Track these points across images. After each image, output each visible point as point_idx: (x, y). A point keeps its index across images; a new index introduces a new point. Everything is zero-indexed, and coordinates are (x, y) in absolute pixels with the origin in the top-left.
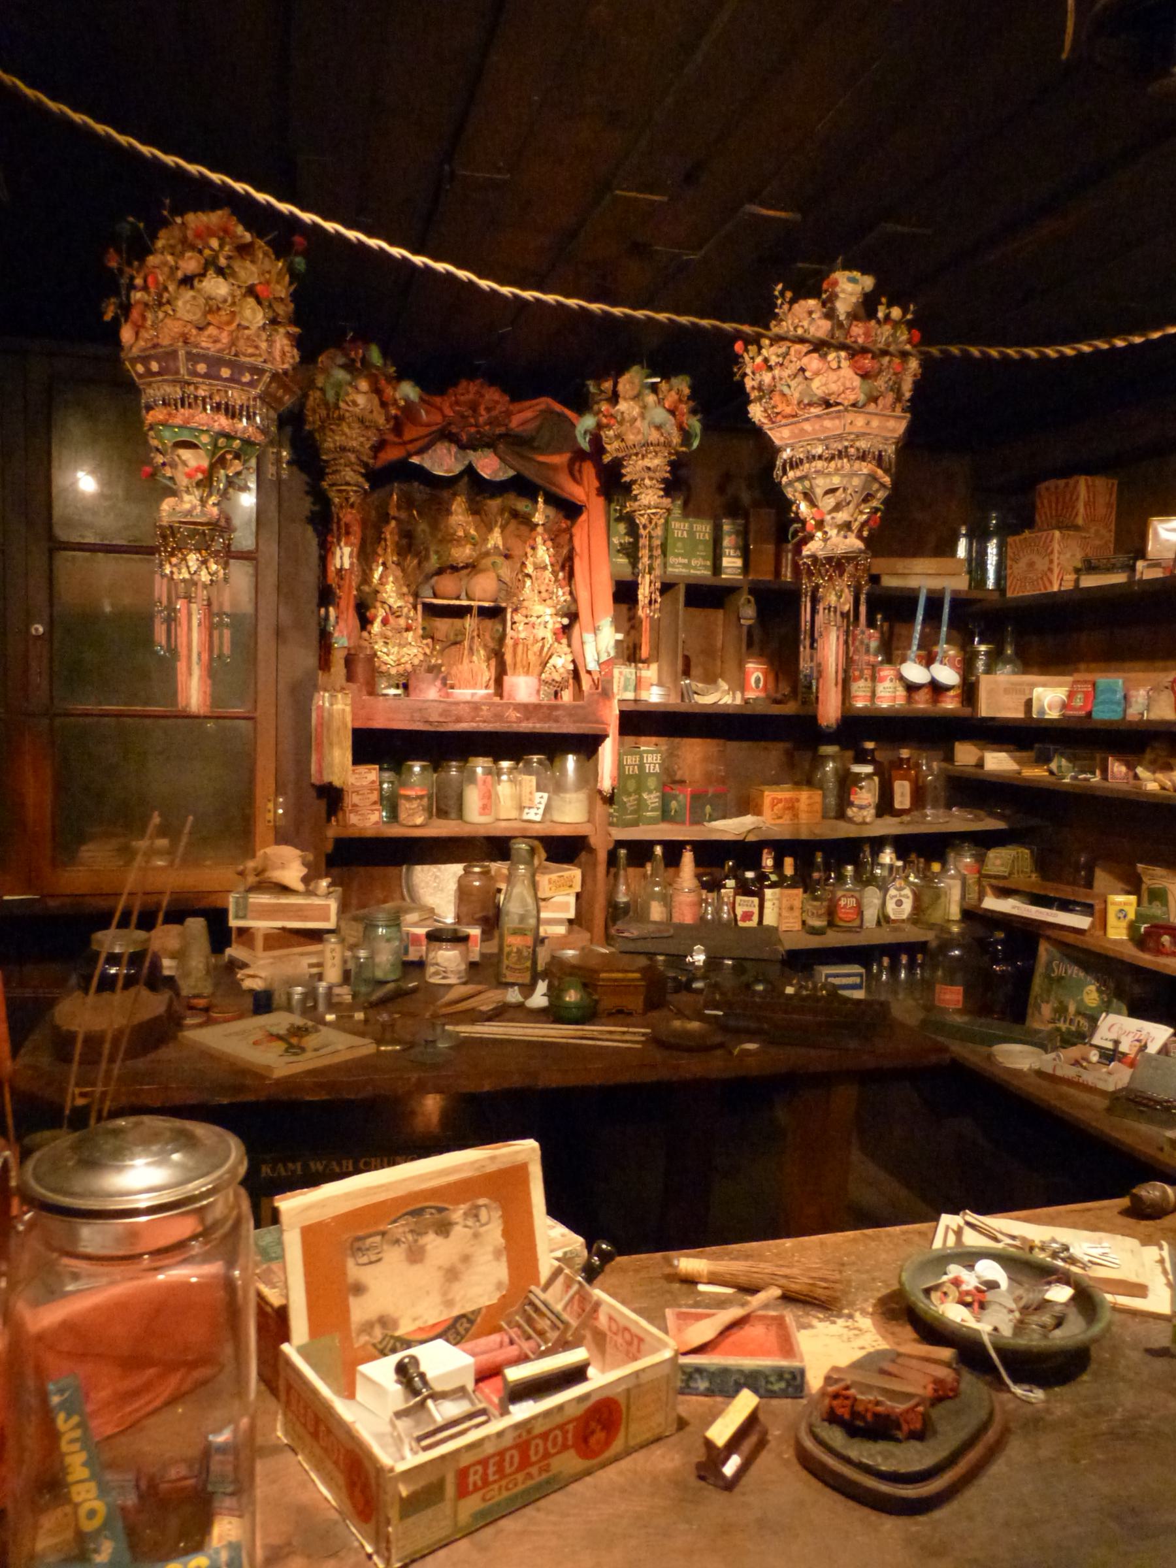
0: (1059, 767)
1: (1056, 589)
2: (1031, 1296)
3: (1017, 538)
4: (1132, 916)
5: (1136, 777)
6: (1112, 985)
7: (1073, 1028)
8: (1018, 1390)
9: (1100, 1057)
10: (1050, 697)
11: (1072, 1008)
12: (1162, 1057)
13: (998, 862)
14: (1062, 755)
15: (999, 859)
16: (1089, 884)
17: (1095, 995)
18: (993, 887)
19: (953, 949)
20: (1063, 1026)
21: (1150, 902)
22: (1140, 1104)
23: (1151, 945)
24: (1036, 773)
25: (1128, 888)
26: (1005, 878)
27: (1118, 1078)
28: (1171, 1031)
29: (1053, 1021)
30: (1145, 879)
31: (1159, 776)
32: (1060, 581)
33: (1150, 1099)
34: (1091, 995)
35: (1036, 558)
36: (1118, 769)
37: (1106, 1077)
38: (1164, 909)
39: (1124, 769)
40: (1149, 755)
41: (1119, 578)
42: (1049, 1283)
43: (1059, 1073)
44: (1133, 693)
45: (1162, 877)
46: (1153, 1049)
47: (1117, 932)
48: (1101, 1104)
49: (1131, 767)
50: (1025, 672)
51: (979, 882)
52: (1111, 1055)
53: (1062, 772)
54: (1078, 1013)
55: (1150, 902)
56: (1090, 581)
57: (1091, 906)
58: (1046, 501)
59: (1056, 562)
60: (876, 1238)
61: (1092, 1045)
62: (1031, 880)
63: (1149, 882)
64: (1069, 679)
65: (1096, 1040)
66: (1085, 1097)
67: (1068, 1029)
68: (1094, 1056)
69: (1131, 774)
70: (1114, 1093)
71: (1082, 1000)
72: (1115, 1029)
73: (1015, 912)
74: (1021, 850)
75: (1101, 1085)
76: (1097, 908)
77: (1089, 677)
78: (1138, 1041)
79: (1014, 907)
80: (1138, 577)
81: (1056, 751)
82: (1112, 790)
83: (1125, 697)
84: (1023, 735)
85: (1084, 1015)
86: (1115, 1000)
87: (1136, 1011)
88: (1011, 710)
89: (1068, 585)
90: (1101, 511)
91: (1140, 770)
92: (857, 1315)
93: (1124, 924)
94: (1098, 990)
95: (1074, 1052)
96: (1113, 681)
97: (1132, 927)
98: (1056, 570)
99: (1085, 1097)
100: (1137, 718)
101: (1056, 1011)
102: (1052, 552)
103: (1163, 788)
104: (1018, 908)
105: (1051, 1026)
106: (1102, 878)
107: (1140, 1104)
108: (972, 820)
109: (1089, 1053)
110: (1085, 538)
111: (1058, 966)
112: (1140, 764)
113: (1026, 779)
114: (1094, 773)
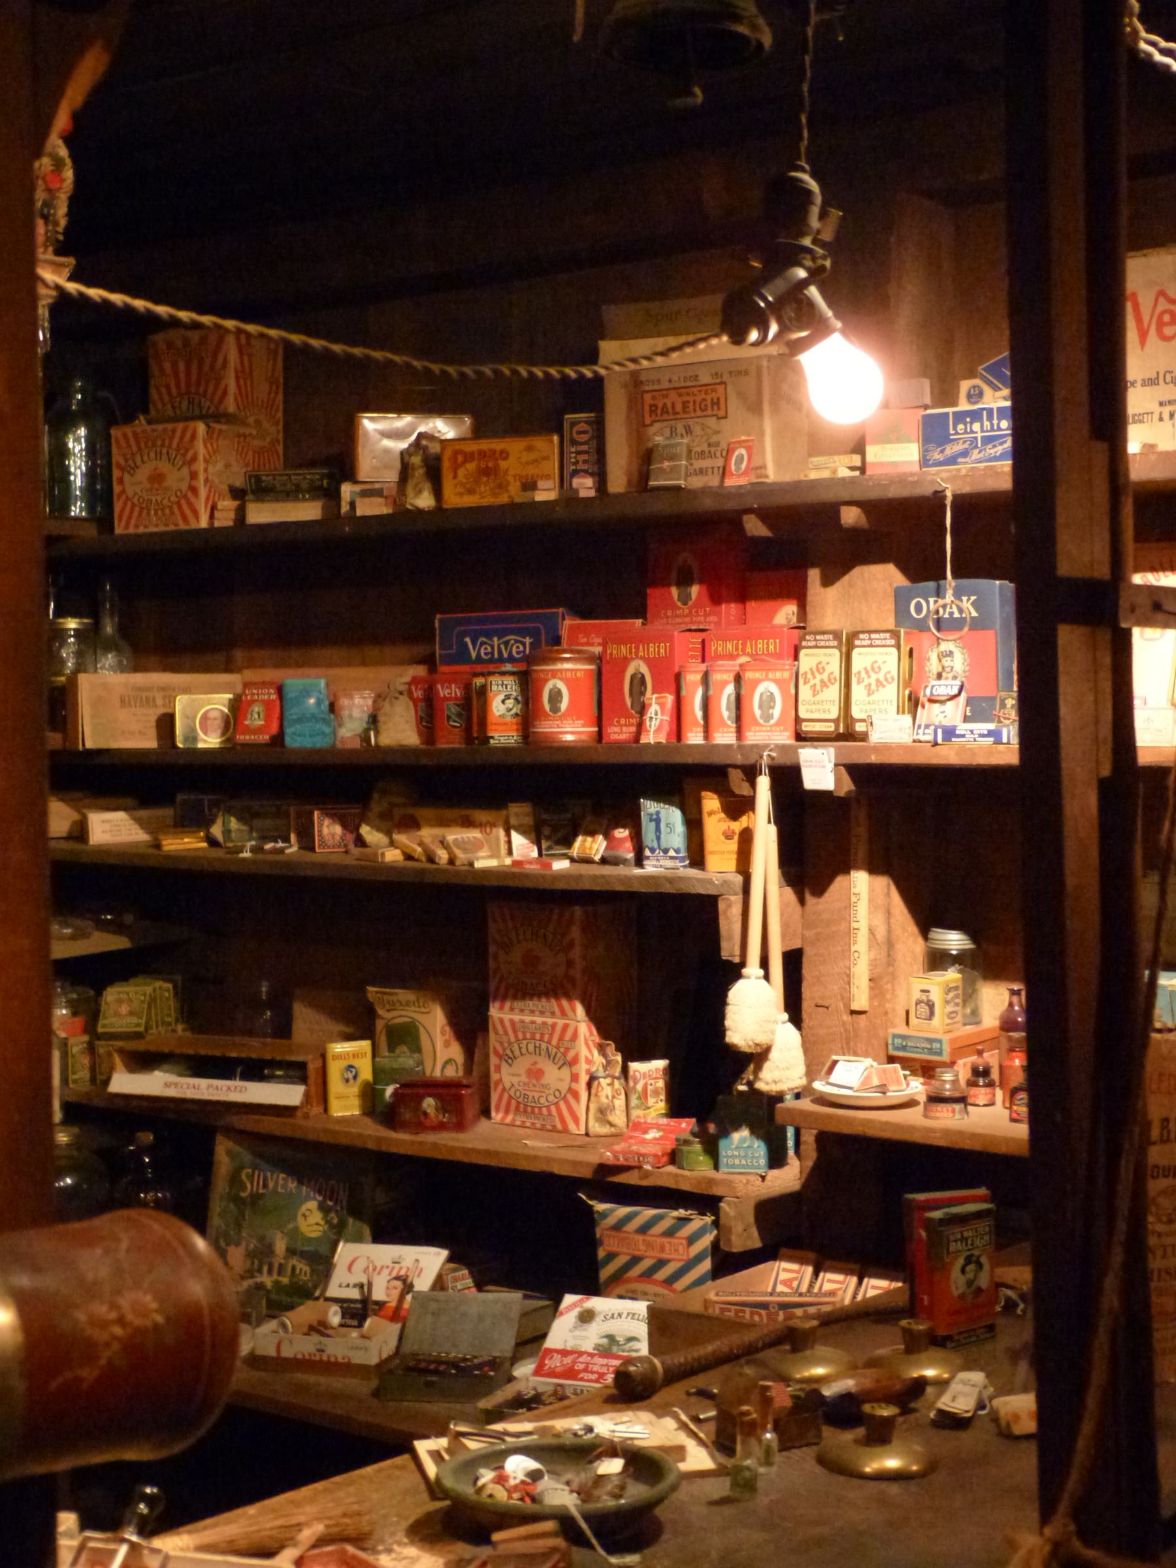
0: (227, 832)
1: (204, 523)
2: (583, 1475)
3: (128, 430)
4: (366, 1074)
5: (360, 842)
6: (343, 1196)
7: (285, 1280)
8: (614, 1560)
9: (343, 1317)
10: (203, 710)
11: (280, 1246)
12: (440, 1295)
13: (124, 1009)
14: (229, 811)
15: (126, 1005)
16: (283, 1029)
17: (317, 1217)
18: (121, 1051)
19: (60, 1175)
20: (267, 1280)
21: (392, 1048)
22: (426, 1371)
23: (407, 1115)
24: (184, 844)
25: (349, 1030)
26: (138, 1036)
27: (378, 1342)
28: (444, 1253)
29: (250, 1273)
30: (380, 1012)
31: (401, 838)
32: (212, 511)
33: (439, 1362)
34: (311, 1218)
35: (164, 466)
36: (329, 830)
37: (360, 1342)
38: (416, 1055)
39: (338, 829)
40: (377, 805)
41: (308, 511)
42: (591, 1462)
43: (287, 1352)
44: (344, 702)
45: (408, 1003)
46: (423, 1284)
47: (345, 1104)
48: (363, 1387)
49: (351, 826)
50: (136, 669)
51: (91, 1049)
52: (359, 1310)
53: (231, 838)
54: (291, 1252)
55: (391, 1049)
56: (261, 514)
57: (302, 1066)
58: (167, 366)
59: (202, 477)
60: (351, 1483)
61: (327, 1299)
62: (173, 1033)
63: (389, 1015)
64: (234, 678)
65: (333, 1291)
66: (337, 1383)
67: (277, 1283)
68: (335, 1317)
69: (350, 837)
70: (378, 1366)
71: (296, 1229)
72: (359, 1266)
73: (171, 1093)
74: (158, 984)
75: (358, 1358)
76: (312, 1067)
77: (270, 674)
78: (397, 1278)
79: (167, 1085)
80: (345, 508)
81: (216, 804)
82: (323, 866)
83: (332, 708)
84: (158, 778)
85: (303, 1255)
86: (351, 1220)
87: (381, 1236)
88: (138, 737)
89: (225, 519)
90: (262, 390)
91: (365, 830)
92: (395, 1547)
93: (355, 1089)
94: (322, 1207)
95: (305, 1313)
96: (309, 687)
97: (370, 1094)
98: (203, 492)
99: (337, 1383)
100: (357, 744)
101: (251, 1255)
102: (194, 459)
103: (409, 857)
104: (176, 1084)
105: (246, 1284)
106: (306, 1020)
107: (426, 1371)
108: (73, 938)
109: (326, 1313)
110: (245, 436)
111: (251, 1177)
112: (363, 819)
113: (168, 857)
114: (286, 839)
